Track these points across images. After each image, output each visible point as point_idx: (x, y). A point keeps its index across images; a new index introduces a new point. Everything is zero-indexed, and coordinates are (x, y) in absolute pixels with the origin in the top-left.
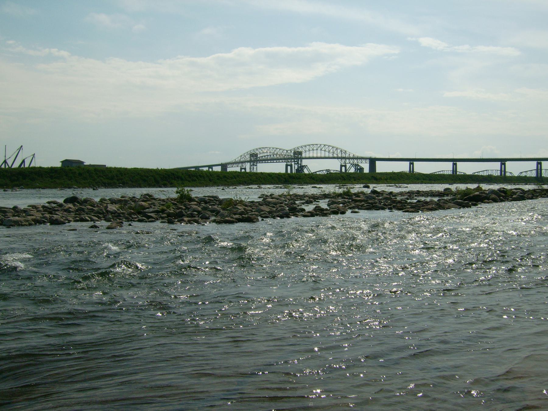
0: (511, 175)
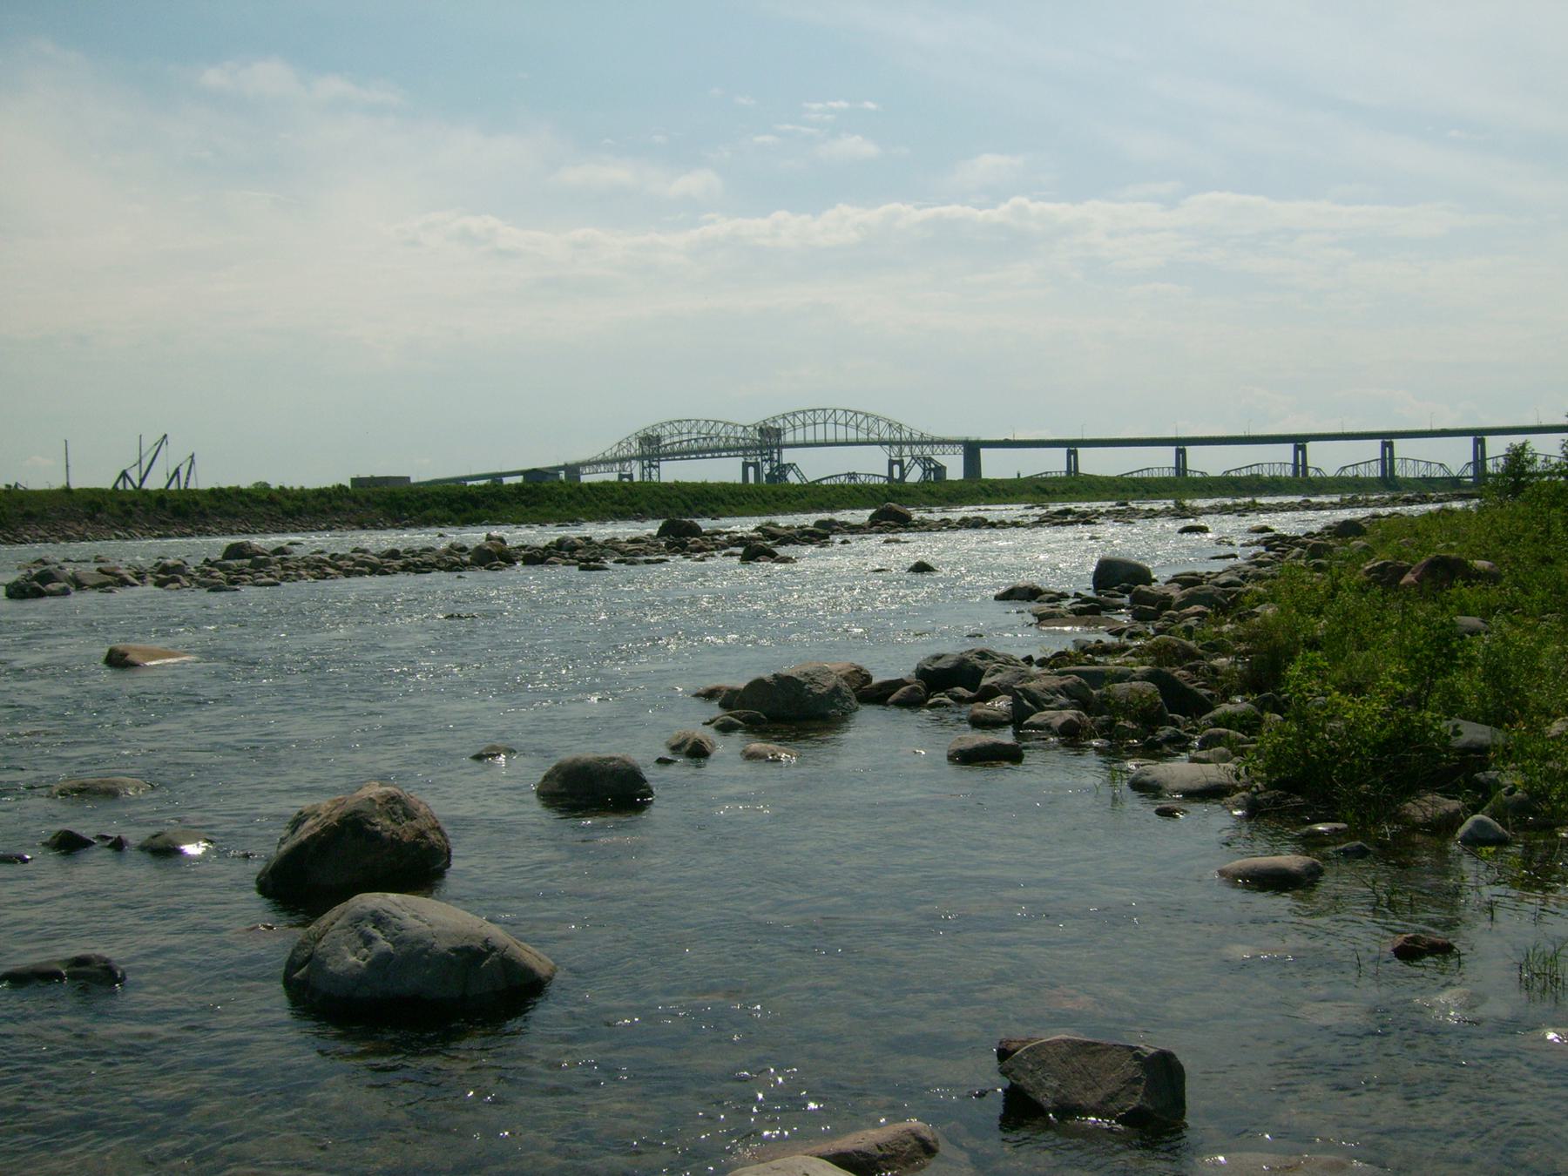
0: (1318, 475)
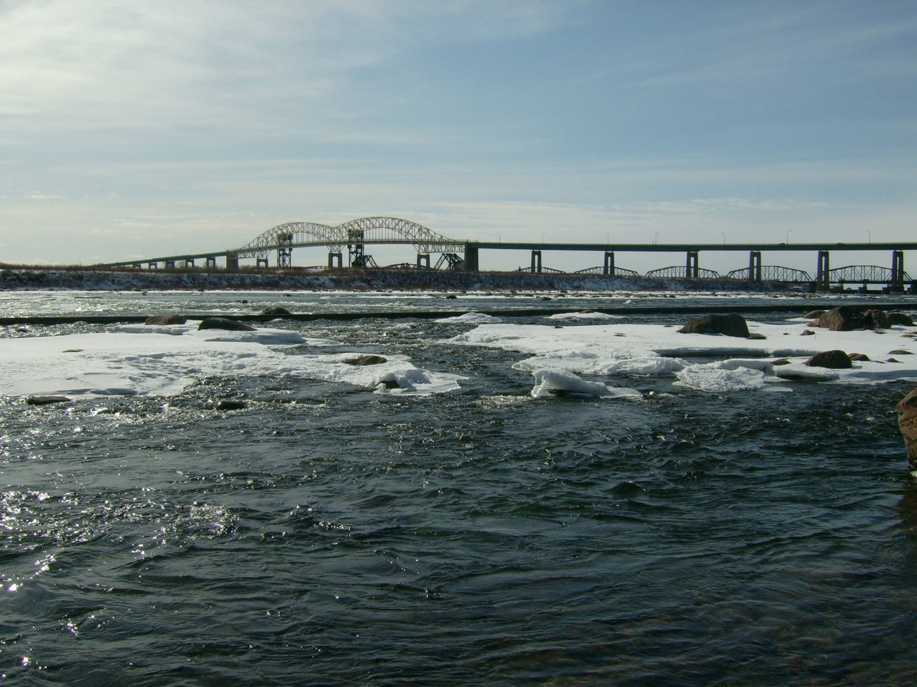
0: (714, 277)
